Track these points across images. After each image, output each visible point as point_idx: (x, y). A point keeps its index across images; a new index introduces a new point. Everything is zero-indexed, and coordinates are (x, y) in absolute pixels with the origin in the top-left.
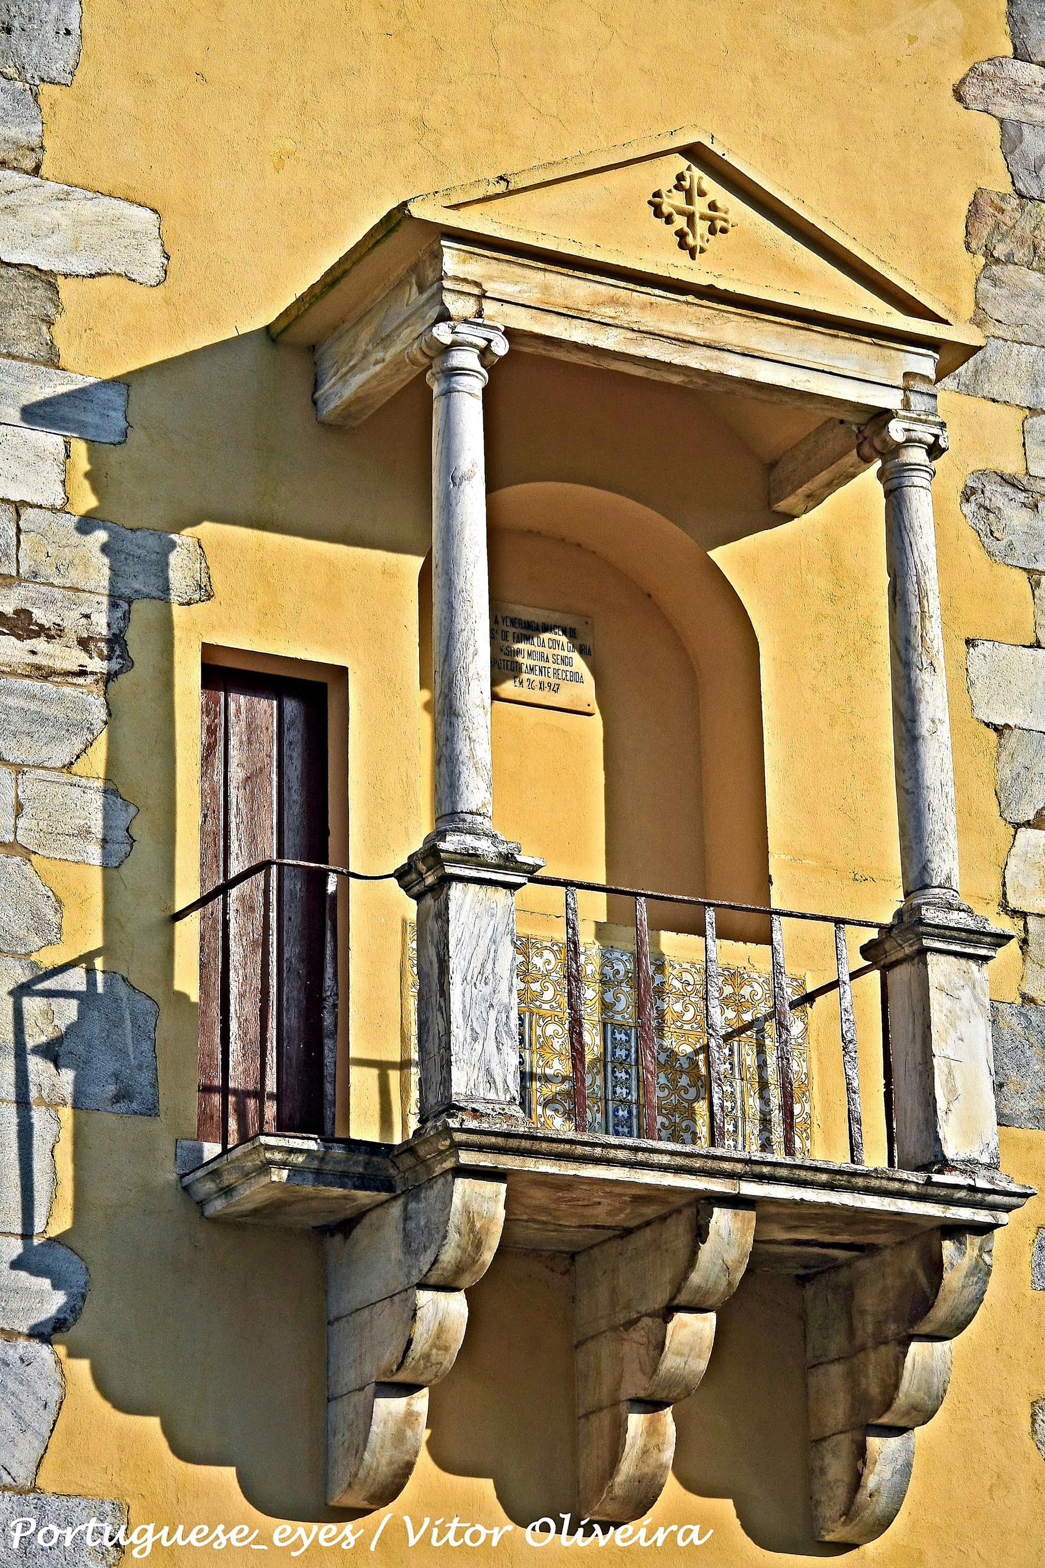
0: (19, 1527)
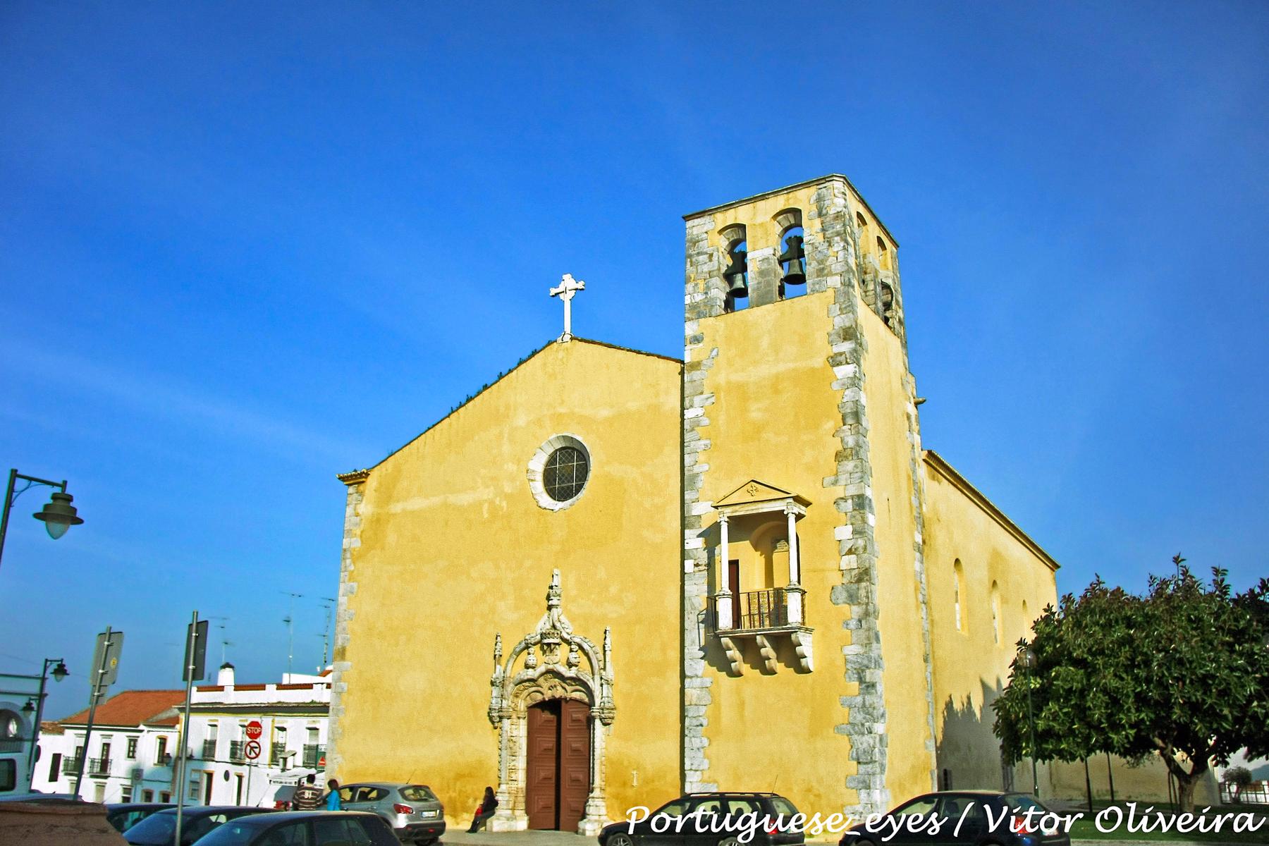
0: (634, 814)
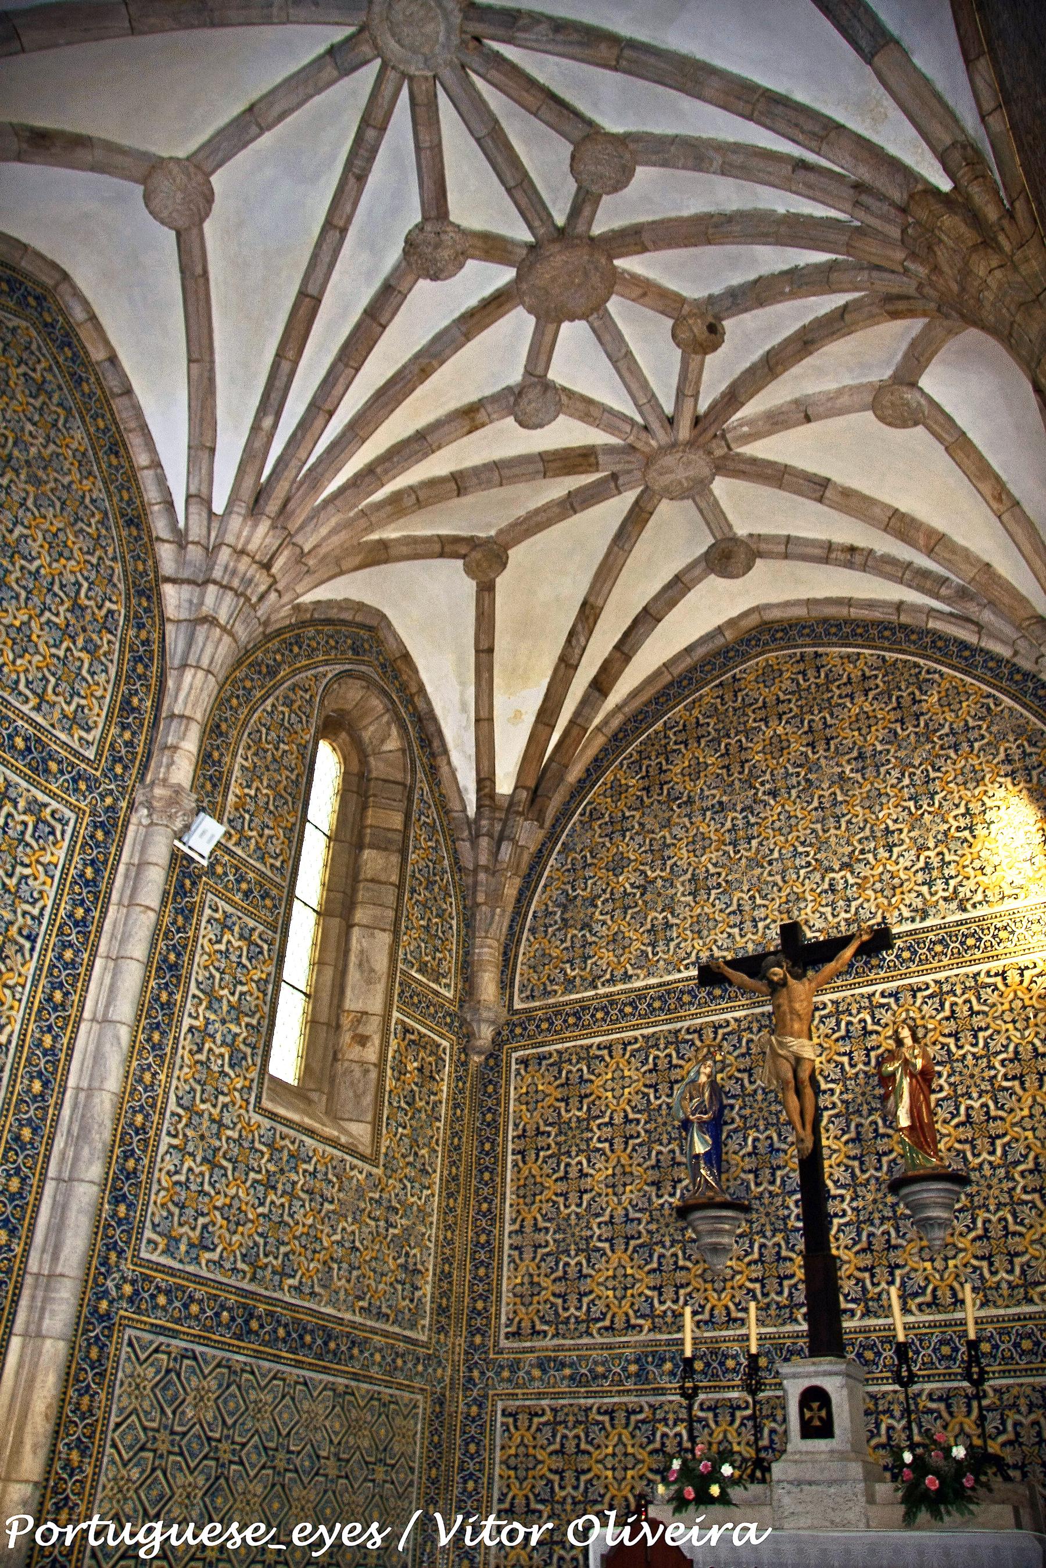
0: (16, 1524)
